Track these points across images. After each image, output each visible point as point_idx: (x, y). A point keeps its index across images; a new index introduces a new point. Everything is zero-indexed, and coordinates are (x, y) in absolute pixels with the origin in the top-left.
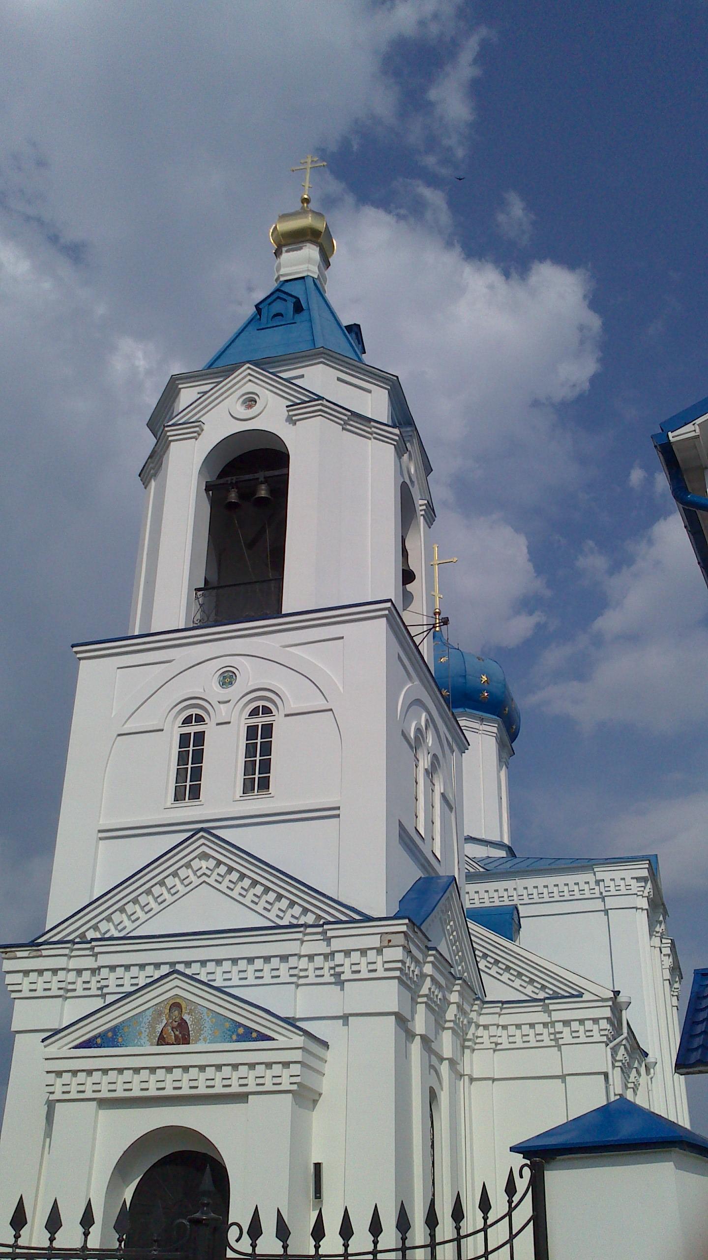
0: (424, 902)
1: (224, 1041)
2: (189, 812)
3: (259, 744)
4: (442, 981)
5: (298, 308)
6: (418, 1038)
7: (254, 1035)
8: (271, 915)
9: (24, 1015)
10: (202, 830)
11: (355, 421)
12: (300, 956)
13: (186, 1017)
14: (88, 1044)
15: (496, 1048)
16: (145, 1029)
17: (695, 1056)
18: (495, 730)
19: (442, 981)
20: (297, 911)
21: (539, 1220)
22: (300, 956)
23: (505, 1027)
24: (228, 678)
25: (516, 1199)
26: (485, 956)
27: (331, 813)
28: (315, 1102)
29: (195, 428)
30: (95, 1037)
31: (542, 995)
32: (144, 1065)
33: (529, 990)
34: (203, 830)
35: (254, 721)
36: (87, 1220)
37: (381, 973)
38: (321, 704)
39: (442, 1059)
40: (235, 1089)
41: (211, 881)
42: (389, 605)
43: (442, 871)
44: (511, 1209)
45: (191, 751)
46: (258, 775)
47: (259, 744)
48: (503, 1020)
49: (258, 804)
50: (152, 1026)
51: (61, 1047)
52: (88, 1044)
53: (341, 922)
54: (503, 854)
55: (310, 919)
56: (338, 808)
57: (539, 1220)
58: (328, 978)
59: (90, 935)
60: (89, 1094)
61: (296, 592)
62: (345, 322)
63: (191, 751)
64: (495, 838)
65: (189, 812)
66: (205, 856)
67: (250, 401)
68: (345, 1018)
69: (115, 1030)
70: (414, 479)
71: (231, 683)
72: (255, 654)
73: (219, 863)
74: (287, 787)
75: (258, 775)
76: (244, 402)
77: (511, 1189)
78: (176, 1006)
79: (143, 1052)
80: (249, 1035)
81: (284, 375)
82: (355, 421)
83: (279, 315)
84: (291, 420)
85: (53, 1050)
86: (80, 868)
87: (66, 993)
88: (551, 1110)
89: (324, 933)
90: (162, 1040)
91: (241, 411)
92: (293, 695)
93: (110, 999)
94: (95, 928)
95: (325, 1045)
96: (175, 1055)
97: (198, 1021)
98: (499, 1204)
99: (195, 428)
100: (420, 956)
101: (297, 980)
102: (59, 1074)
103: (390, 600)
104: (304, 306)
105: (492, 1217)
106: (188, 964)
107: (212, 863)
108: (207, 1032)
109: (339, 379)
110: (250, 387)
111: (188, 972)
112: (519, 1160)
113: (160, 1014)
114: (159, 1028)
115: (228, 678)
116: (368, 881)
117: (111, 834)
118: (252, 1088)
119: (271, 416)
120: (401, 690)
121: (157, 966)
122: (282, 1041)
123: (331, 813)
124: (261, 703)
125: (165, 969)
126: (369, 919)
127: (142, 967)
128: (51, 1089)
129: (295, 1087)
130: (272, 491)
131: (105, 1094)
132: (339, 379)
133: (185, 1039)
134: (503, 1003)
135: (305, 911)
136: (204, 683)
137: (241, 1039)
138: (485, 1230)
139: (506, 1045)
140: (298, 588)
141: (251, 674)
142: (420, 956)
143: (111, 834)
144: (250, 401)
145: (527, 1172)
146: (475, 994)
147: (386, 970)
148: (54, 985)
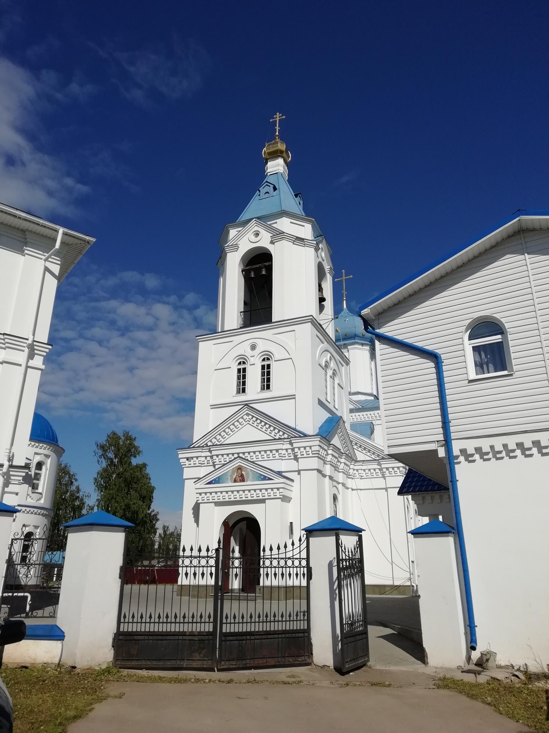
0: (330, 428)
1: (257, 481)
2: (242, 398)
3: (266, 371)
4: (337, 455)
5: (275, 189)
6: (328, 477)
7: (267, 478)
8: (272, 435)
9: (187, 473)
10: (246, 405)
11: (299, 240)
12: (283, 449)
13: (243, 473)
14: (210, 483)
15: (362, 478)
16: (229, 478)
17: (405, 490)
18: (368, 348)
19: (337, 455)
20: (281, 433)
21: (308, 547)
22: (283, 449)
23: (364, 470)
24: (253, 347)
25: (301, 543)
26: (356, 444)
27: (292, 397)
28: (290, 501)
29: (236, 247)
30: (212, 481)
31: (378, 458)
32: (230, 489)
33: (373, 456)
34: (247, 405)
35: (264, 363)
36: (192, 549)
37: (311, 455)
38: (288, 356)
39: (339, 483)
40: (261, 497)
41: (250, 423)
42: (311, 317)
43: (339, 414)
44: (300, 545)
45: (242, 374)
46: (266, 385)
47: (266, 371)
48: (363, 468)
49: (267, 394)
50: (232, 476)
51: (201, 484)
52: (210, 483)
53: (296, 437)
54: (372, 398)
55: (286, 436)
56: (295, 395)
57: (308, 547)
58: (293, 457)
59: (209, 444)
60: (211, 501)
61: (276, 316)
62: (105, 654)
63: (242, 374)
64: (369, 391)
65: (242, 398)
66: (248, 414)
67: (257, 235)
68: (299, 472)
69: (218, 478)
70: (324, 259)
71: (255, 349)
72: (263, 338)
73: (253, 417)
74: (277, 389)
75: (266, 385)
76: (254, 235)
77: (300, 540)
78: (240, 468)
79: (229, 485)
80: (265, 478)
81: (268, 223)
82: (299, 240)
83: (268, 193)
84: (272, 243)
85: (198, 486)
86: (205, 421)
87: (201, 465)
88: (311, 520)
89: (291, 441)
90: (235, 481)
91: (253, 239)
92: (278, 353)
93: (217, 467)
94: (211, 441)
95: (292, 480)
96: (240, 486)
97: (247, 474)
98: (297, 543)
99: (236, 247)
100: (326, 448)
101: (282, 458)
102: (200, 494)
103: (312, 316)
104: (277, 187)
105: (295, 547)
106: (244, 453)
107: (250, 417)
108: (251, 478)
109: (291, 222)
110: (256, 228)
111: (244, 457)
112: (304, 532)
113: (234, 472)
114: (234, 477)
115: (253, 347)
116: (309, 421)
117: (214, 407)
118: (267, 497)
119: (264, 241)
120: (317, 350)
121: (233, 454)
122: (276, 481)
123: (292, 397)
124: (266, 356)
125: (236, 456)
126: (305, 436)
127: (228, 455)
128: (198, 499)
129: (281, 497)
130: (266, 271)
131: (216, 500)
132: (291, 222)
133: (243, 480)
134: (363, 461)
135: (284, 433)
136: (245, 349)
137: (263, 480)
138: (293, 550)
139: (365, 477)
140: (278, 312)
141: (262, 346)
142: (326, 448)
143: (214, 407)
144: (257, 235)
145: (305, 536)
146: (352, 458)
147: (313, 454)
148: (197, 462)
